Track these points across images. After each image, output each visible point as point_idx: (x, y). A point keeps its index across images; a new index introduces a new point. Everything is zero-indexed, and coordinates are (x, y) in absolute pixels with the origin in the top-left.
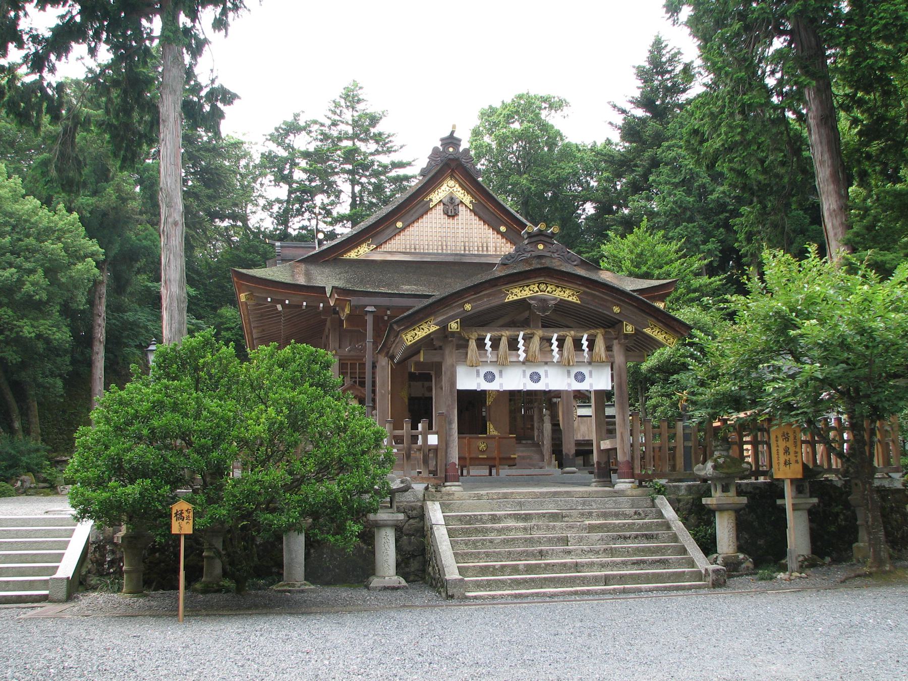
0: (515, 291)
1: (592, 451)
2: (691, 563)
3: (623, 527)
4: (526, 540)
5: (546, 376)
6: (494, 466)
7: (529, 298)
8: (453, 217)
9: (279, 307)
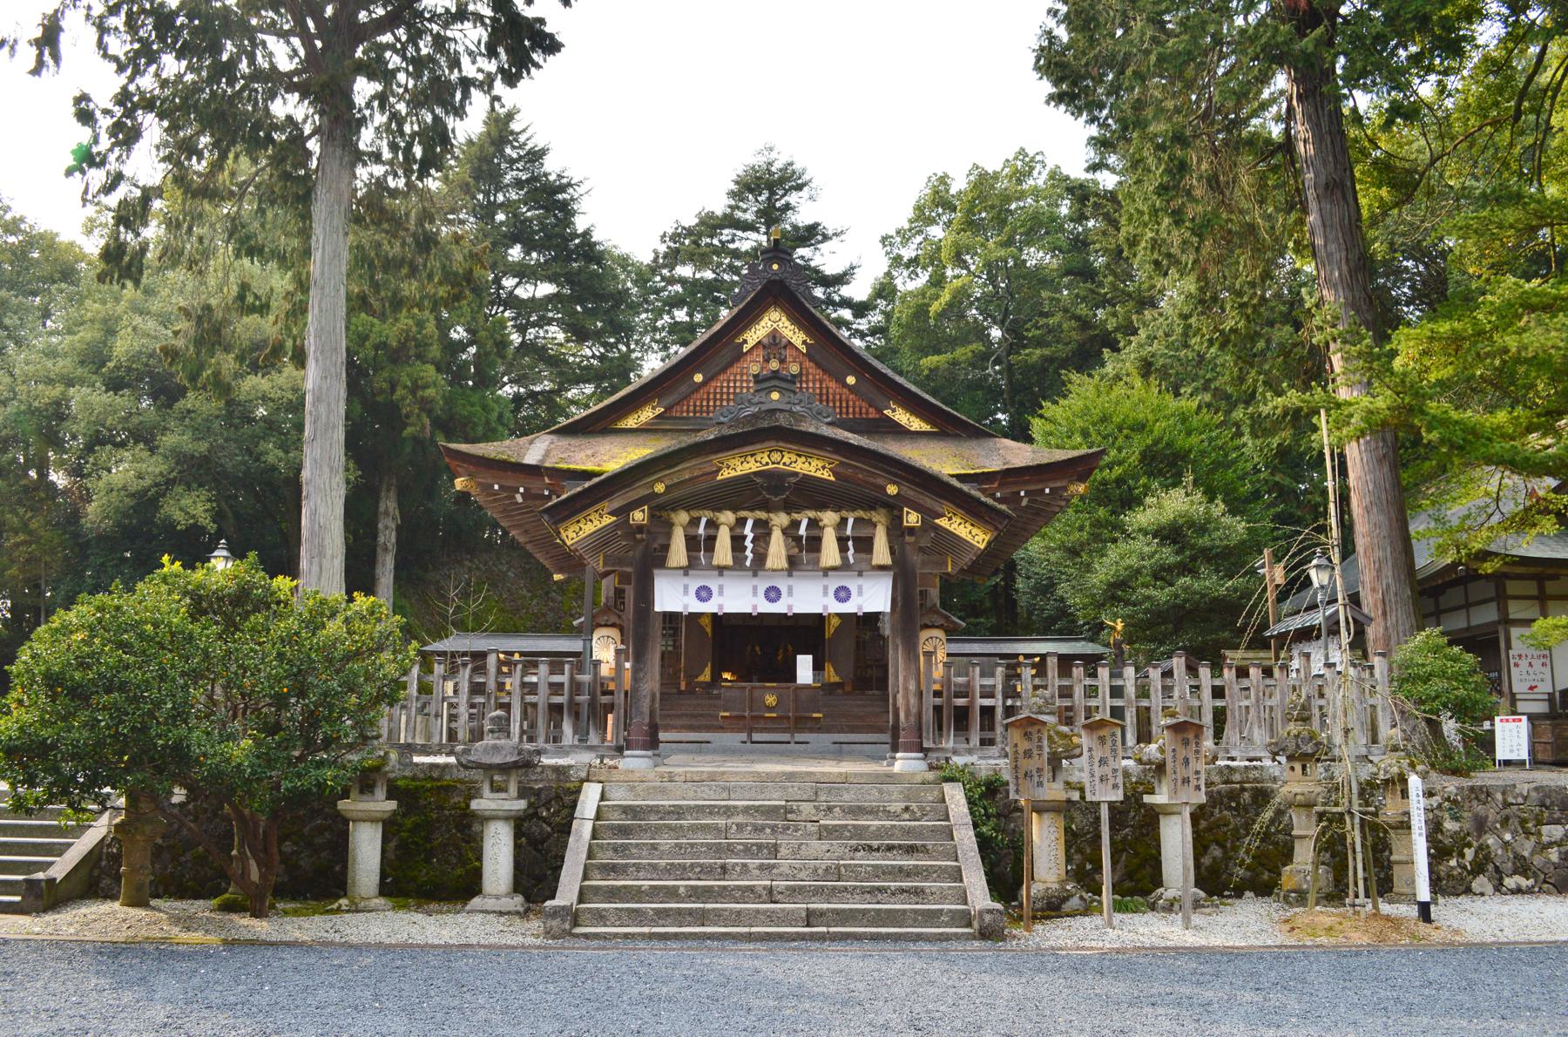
0: (731, 463)
3: (880, 833)
5: (860, 593)
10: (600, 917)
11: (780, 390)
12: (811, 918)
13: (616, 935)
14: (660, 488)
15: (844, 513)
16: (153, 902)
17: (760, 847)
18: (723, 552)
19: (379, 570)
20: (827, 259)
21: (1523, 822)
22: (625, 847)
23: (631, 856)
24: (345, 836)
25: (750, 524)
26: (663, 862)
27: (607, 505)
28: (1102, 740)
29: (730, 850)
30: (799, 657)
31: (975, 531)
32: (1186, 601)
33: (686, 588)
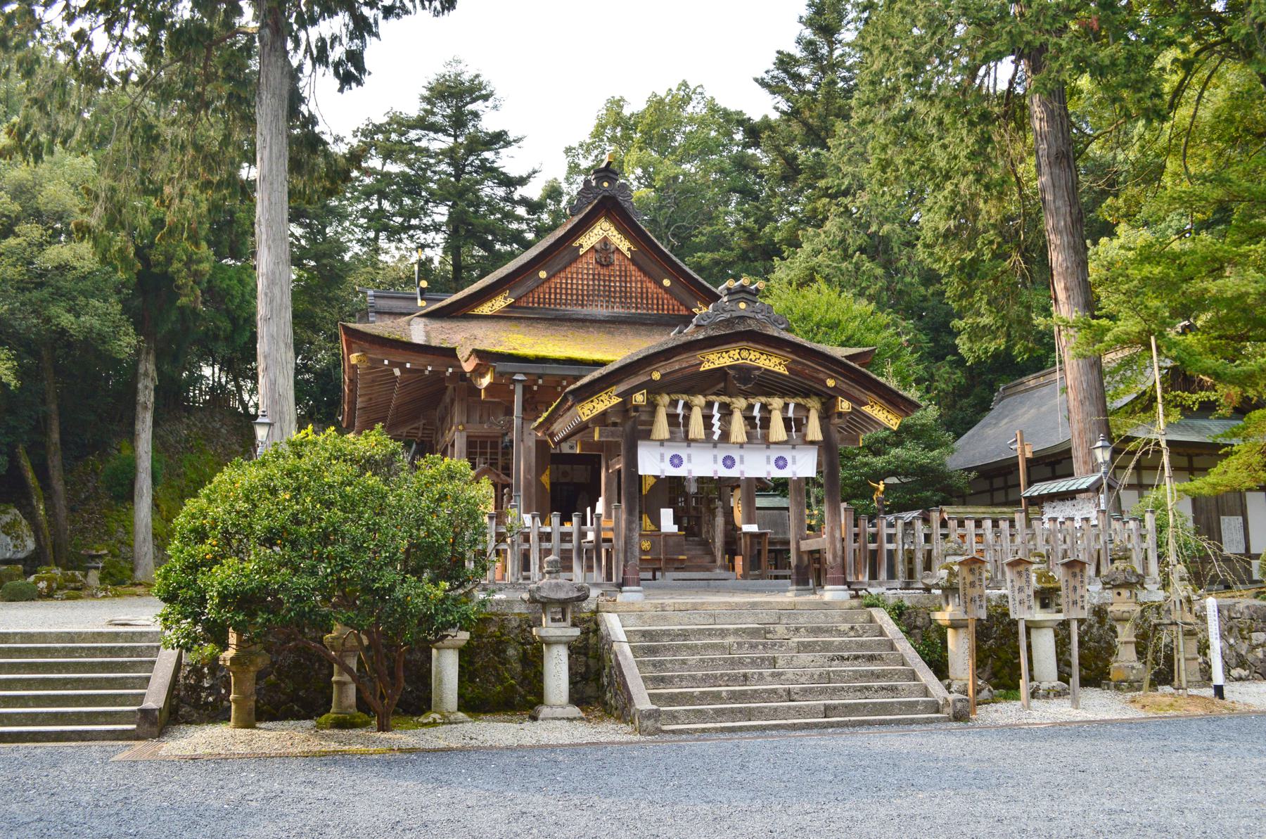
0: (711, 357)
1: (788, 551)
2: (926, 692)
3: (841, 647)
4: (725, 660)
5: (794, 462)
6: (659, 569)
7: (729, 367)
8: (607, 266)
9: (397, 372)
10: (673, 717)
11: (747, 301)
12: (828, 711)
13: (696, 730)
14: (656, 376)
15: (787, 400)
16: (258, 725)
17: (763, 659)
18: (697, 427)
19: (139, 426)
20: (509, 161)
21: (1241, 630)
22: (662, 663)
23: (667, 670)
24: (540, 657)
25: (716, 406)
26: (700, 673)
27: (616, 389)
28: (1019, 573)
29: (740, 662)
30: (662, 510)
31: (890, 416)
32: (898, 467)
33: (662, 456)
